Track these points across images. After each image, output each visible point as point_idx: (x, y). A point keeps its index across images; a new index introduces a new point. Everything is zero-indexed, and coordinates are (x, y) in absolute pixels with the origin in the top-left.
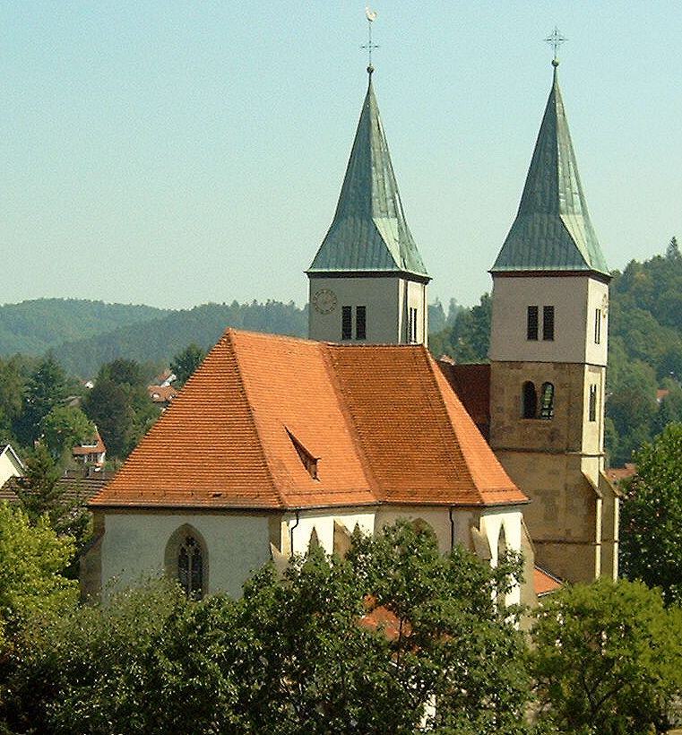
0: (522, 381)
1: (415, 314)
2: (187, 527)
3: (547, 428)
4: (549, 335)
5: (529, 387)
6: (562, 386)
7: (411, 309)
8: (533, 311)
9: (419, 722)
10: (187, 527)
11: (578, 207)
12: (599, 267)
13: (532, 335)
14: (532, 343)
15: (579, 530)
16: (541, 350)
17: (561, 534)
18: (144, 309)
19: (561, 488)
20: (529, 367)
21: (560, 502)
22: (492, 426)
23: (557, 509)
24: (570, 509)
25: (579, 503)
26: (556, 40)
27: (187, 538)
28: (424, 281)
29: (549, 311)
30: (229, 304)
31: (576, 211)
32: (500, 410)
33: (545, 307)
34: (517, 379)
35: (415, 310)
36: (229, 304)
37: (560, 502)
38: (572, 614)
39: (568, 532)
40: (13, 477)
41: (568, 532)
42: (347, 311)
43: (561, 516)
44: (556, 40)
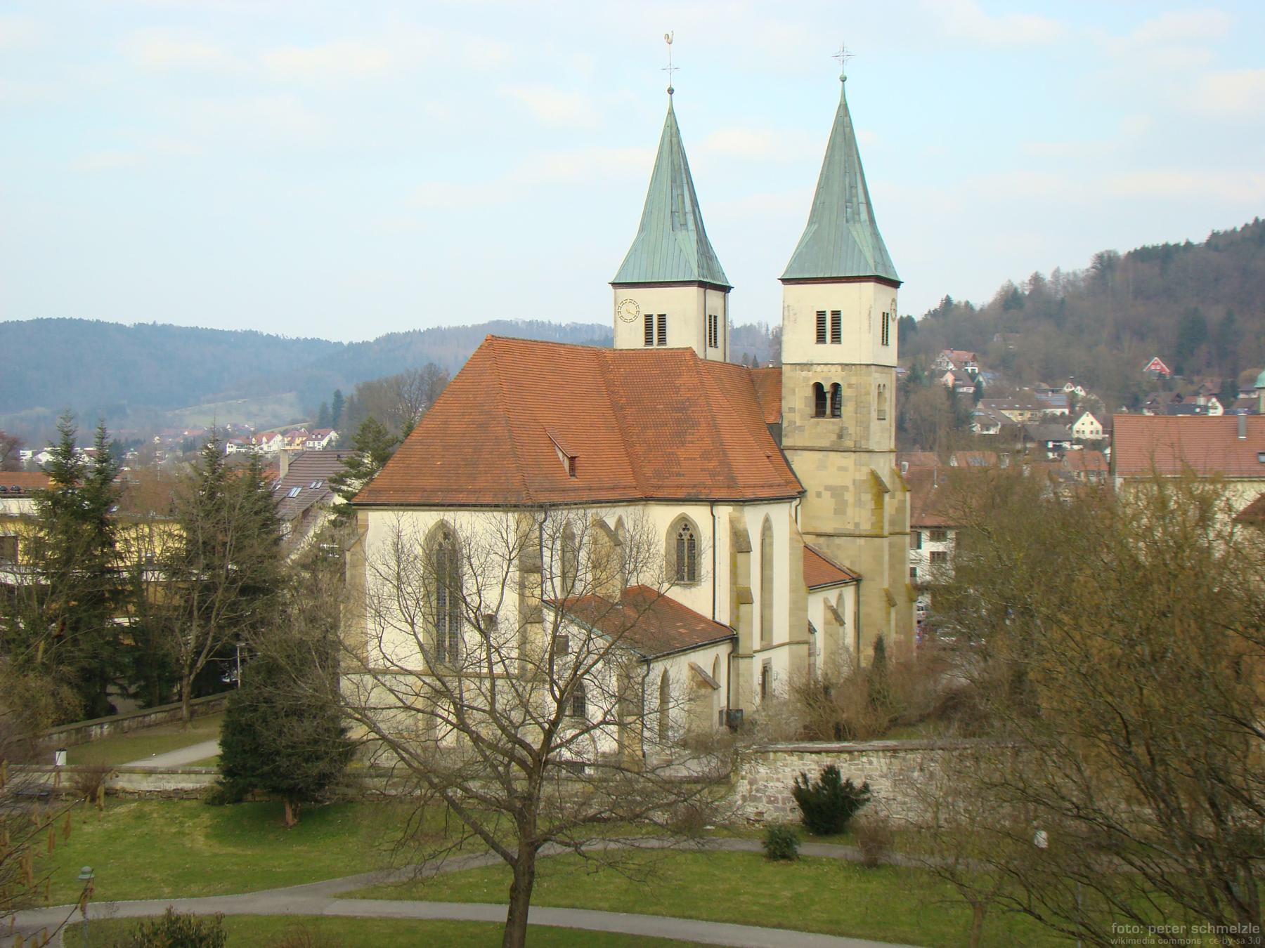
0: (812, 382)
2: (442, 525)
3: (236, 868)
4: (836, 337)
5: (818, 387)
6: (850, 386)
7: (710, 316)
8: (821, 316)
10: (442, 525)
11: (864, 216)
13: (821, 338)
14: (821, 346)
15: (698, 726)
16: (829, 352)
18: (315, 343)
19: (849, 484)
20: (819, 369)
22: (784, 426)
23: (846, 502)
24: (859, 503)
26: (843, 56)
27: (445, 534)
29: (836, 315)
30: (411, 331)
31: (862, 220)
32: (792, 410)
34: (807, 379)
35: (715, 317)
36: (411, 331)
37: (849, 497)
39: (857, 525)
40: (689, 350)
41: (857, 525)
42: (648, 318)
44: (843, 56)
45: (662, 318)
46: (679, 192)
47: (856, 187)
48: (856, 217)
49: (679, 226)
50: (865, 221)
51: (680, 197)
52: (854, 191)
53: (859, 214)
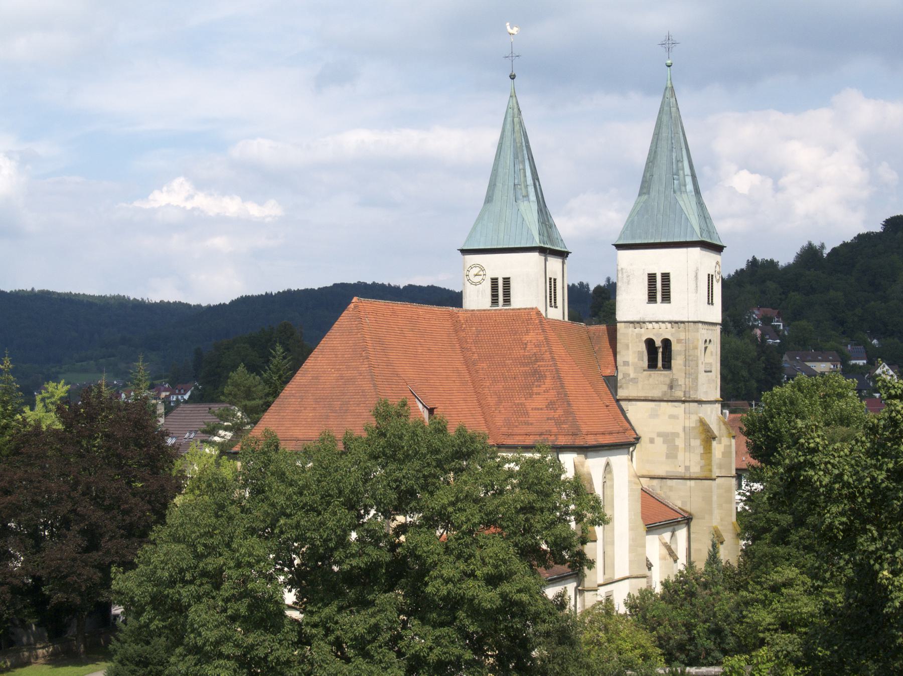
0: (644, 339)
1: (712, 278)
4: (666, 298)
5: (650, 343)
6: (679, 341)
8: (652, 278)
9: (665, 659)
12: (552, 243)
13: (652, 298)
14: (652, 305)
16: (659, 310)
17: (681, 471)
19: (679, 430)
20: (650, 326)
21: (680, 442)
24: (688, 448)
25: (697, 443)
28: (563, 255)
29: (666, 277)
30: (264, 294)
32: (626, 363)
33: (504, 279)
36: (264, 294)
37: (680, 442)
38: (473, 452)
39: (687, 468)
41: (687, 468)
42: (494, 281)
43: (681, 455)
45: (507, 281)
46: (521, 167)
47: (682, 161)
48: (683, 188)
49: (521, 197)
50: (691, 192)
51: (522, 171)
52: (680, 165)
53: (685, 185)
